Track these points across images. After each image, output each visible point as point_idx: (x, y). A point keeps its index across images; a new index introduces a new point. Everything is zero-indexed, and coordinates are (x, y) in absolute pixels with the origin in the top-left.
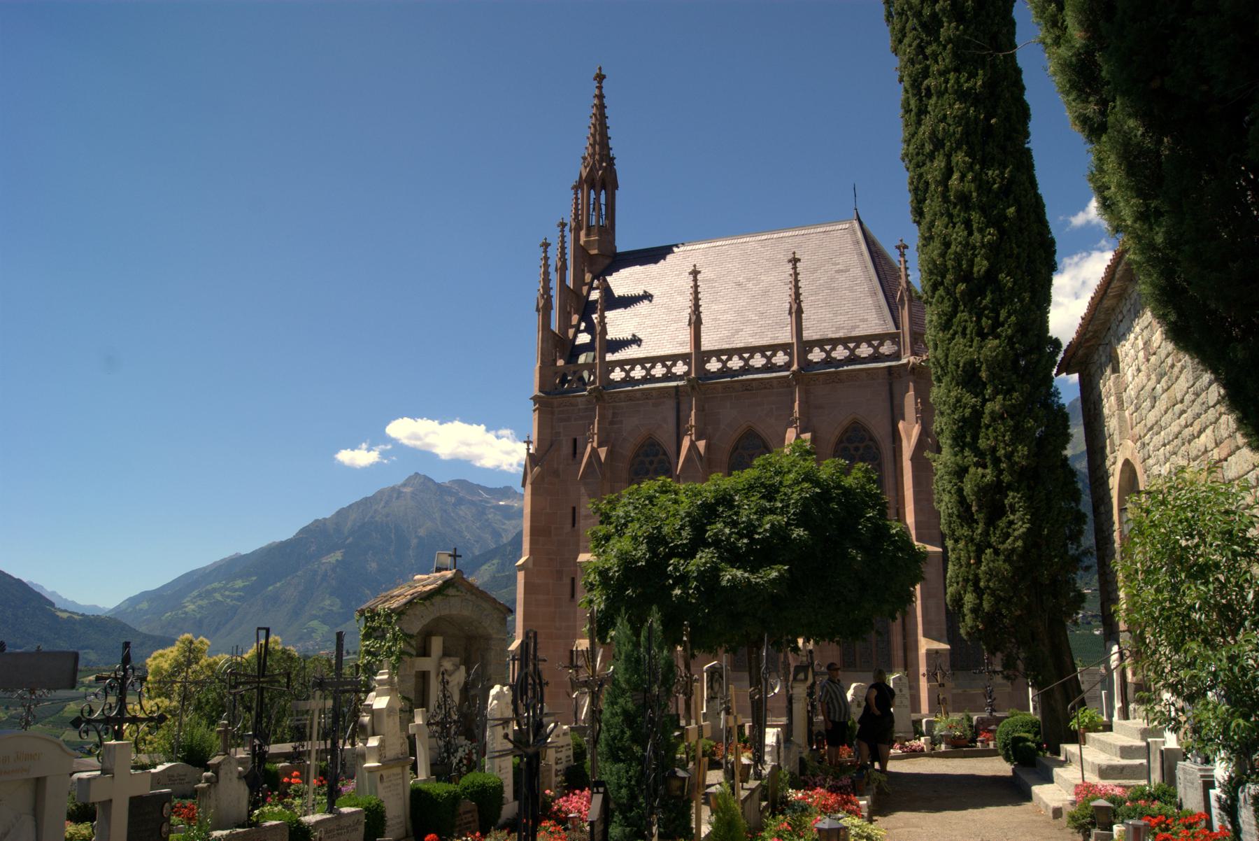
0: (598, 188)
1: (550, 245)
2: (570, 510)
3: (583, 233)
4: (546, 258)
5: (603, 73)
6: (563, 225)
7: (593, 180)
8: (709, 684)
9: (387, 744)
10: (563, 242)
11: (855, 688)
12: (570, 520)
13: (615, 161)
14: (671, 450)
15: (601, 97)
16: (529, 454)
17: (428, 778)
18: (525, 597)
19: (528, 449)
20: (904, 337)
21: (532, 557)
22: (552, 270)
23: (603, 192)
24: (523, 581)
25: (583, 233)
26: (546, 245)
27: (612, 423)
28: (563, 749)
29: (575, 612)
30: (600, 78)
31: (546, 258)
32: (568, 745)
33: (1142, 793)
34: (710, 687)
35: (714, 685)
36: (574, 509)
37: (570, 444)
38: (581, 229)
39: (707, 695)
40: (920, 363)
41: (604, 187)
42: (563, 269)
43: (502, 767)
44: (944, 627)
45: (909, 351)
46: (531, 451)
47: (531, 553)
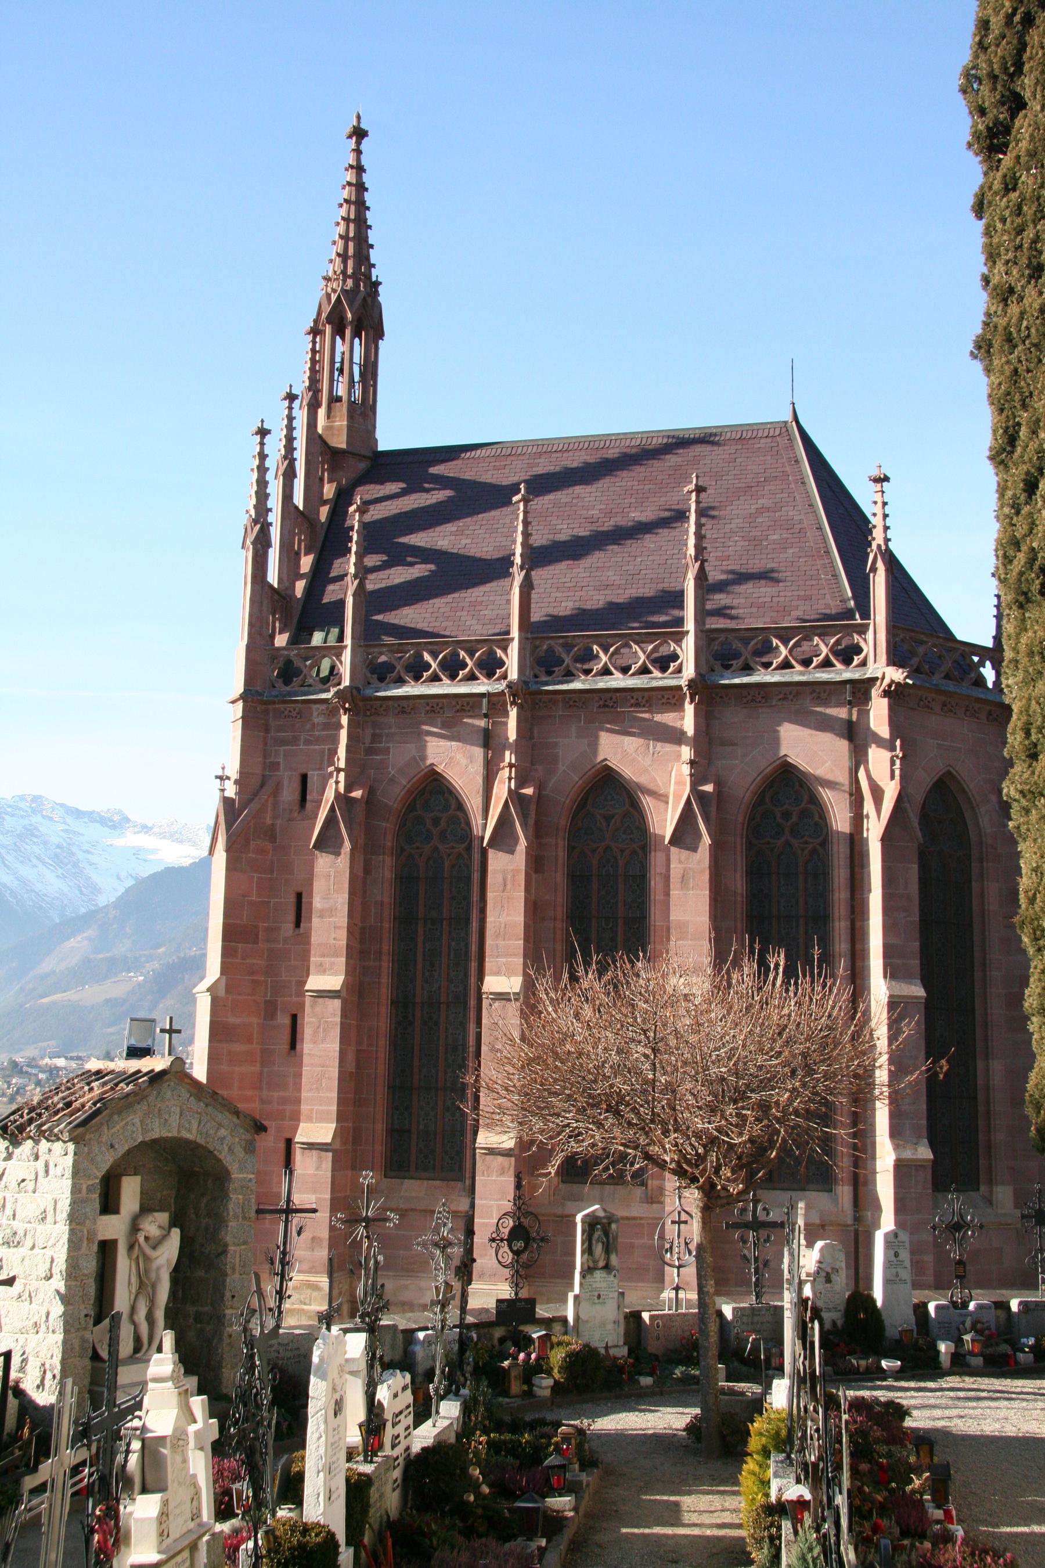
0: (348, 333)
1: (268, 432)
2: (292, 899)
4: (263, 456)
5: (363, 126)
6: (291, 397)
8: (586, 1245)
10: (290, 428)
12: (291, 917)
13: (380, 289)
14: (473, 802)
18: (210, 1047)
26: (263, 432)
27: (370, 751)
28: (402, 1417)
30: (359, 134)
31: (263, 456)
34: (588, 1250)
35: (594, 1247)
36: (299, 896)
39: (582, 1264)
46: (227, 794)
47: (225, 969)
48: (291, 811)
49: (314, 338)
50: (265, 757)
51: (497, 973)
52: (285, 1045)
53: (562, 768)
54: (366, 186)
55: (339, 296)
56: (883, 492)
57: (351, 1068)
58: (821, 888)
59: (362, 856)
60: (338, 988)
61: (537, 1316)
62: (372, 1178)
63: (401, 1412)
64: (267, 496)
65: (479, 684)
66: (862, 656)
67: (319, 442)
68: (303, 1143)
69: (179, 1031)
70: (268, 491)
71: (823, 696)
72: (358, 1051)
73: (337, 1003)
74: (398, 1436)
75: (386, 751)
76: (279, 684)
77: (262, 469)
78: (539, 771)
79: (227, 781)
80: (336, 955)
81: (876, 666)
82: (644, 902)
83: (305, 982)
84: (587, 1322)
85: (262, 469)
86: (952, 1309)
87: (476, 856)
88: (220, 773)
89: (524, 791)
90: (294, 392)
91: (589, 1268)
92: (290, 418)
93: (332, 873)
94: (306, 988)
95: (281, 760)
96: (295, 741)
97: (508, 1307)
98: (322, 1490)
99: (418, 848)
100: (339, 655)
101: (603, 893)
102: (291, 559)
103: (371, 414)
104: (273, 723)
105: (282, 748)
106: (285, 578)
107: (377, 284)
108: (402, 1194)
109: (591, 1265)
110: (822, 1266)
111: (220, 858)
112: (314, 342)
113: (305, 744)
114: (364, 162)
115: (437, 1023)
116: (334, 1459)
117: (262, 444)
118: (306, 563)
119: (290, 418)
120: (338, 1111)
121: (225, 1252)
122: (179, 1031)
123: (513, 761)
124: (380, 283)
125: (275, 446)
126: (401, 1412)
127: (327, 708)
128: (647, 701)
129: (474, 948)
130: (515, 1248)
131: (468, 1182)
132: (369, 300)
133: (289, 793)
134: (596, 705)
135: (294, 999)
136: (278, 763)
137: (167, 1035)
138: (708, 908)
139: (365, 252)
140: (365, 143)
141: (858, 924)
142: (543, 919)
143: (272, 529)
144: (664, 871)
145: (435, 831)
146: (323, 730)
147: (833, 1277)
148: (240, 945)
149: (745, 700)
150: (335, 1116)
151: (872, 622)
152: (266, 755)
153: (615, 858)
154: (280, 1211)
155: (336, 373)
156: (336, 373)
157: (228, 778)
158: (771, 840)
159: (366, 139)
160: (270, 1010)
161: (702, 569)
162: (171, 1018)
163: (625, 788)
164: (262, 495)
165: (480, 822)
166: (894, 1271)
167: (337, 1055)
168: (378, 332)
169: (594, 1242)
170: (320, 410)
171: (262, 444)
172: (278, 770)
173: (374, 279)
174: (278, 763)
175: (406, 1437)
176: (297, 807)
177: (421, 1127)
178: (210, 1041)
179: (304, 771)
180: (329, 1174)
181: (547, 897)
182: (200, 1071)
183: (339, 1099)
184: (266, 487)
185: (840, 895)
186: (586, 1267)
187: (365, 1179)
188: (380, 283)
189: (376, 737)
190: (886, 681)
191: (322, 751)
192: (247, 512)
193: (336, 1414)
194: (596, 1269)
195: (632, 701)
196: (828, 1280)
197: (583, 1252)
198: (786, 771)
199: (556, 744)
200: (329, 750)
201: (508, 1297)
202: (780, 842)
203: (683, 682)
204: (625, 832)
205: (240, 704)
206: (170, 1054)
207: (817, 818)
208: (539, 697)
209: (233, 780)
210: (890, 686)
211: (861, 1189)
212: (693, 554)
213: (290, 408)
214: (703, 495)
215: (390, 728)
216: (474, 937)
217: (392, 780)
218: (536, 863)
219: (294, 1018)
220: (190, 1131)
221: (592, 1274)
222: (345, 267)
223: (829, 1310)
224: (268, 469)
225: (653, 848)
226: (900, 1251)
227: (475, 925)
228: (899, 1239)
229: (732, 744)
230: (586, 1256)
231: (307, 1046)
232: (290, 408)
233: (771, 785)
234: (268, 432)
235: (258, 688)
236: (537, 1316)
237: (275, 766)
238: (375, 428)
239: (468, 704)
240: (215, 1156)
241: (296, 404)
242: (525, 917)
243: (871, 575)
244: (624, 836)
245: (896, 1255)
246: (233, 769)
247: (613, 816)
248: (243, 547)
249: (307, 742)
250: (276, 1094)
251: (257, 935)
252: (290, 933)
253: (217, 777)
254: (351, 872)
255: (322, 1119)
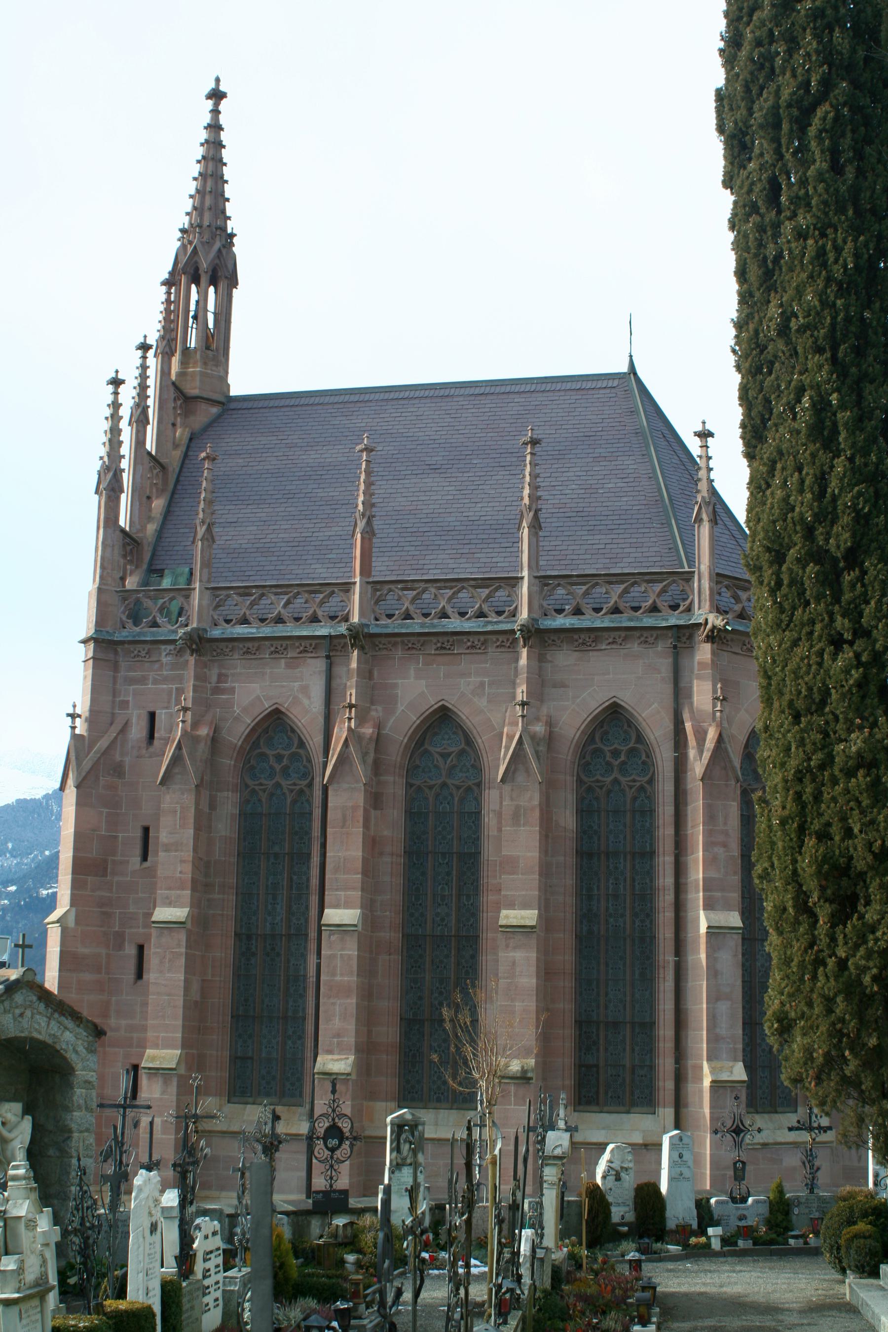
0: (204, 280)
1: (122, 382)
2: (139, 834)
3: (175, 361)
4: (116, 405)
5: (222, 88)
6: (144, 347)
7: (197, 269)
8: (394, 1145)
9: (26, 1265)
10: (143, 377)
11: (612, 1151)
12: (138, 850)
13: (235, 240)
14: (315, 741)
15: (215, 127)
16: (74, 737)
17: (57, 1306)
18: (60, 976)
19: (73, 728)
20: (699, 581)
21: (74, 909)
22: (124, 425)
23: (212, 289)
24: (58, 949)
25: (175, 361)
26: (116, 382)
27: (217, 690)
28: (212, 1256)
29: (145, 1004)
30: (217, 95)
31: (116, 405)
32: (218, 1249)
33: (808, 897)
34: (397, 1149)
35: (402, 1146)
36: (146, 830)
37: (144, 723)
38: (172, 353)
39: (391, 1161)
40: (724, 626)
41: (214, 281)
42: (140, 419)
43: (150, 1288)
44: (740, 1046)
45: (708, 603)
46: (77, 731)
47: (74, 902)
48: (140, 748)
49: (170, 289)
50: (114, 696)
51: (337, 906)
52: (131, 975)
53: (400, 708)
54: (224, 143)
55: (195, 247)
56: (708, 447)
57: (195, 995)
58: (648, 824)
59: (208, 793)
60: (184, 920)
61: (350, 1206)
62: (200, 1080)
63: (211, 1252)
64: (120, 443)
65: (322, 627)
66: (687, 602)
67: (172, 389)
68: (150, 1069)
69: (30, 947)
70: (121, 438)
71: (651, 640)
72: (203, 981)
73: (183, 936)
74: (209, 1270)
75: (232, 691)
76: (129, 624)
77: (115, 417)
78: (377, 712)
79: (78, 720)
80: (183, 888)
81: (700, 612)
82: (478, 838)
83: (152, 914)
84: (396, 1212)
85: (115, 417)
86: (731, 1204)
87: (317, 793)
88: (71, 711)
89: (363, 730)
90: (148, 342)
91: (398, 1164)
92: (144, 367)
93: (179, 809)
94: (154, 919)
95: (130, 699)
96: (143, 680)
97: (323, 1197)
98: (141, 1287)
99: (261, 784)
100: (187, 597)
101: (440, 829)
102: (142, 498)
103: (223, 360)
104: (123, 665)
105: (131, 687)
106: (136, 519)
107: (232, 236)
108: (245, 1118)
109: (399, 1161)
110: (613, 1165)
111: (71, 793)
112: (169, 293)
113: (153, 683)
114: (223, 120)
115: (278, 955)
116: (151, 1266)
117: (116, 393)
118: (158, 504)
119: (144, 367)
120: (183, 1037)
121: (69, 1138)
122: (30, 947)
123: (353, 702)
124: (235, 235)
125: (128, 395)
126: (211, 1252)
127: (175, 649)
128: (482, 644)
129: (315, 881)
130: (330, 1146)
131: (308, 1107)
132: (224, 251)
133: (137, 731)
134: (434, 647)
135: (141, 930)
136: (127, 702)
137: (20, 950)
138: (537, 844)
139: (221, 207)
140: (224, 105)
141: (682, 859)
142: (381, 854)
143: (125, 476)
144: (497, 808)
145: (278, 767)
146: (171, 670)
147: (623, 1175)
148: (89, 878)
149: (576, 643)
150: (179, 1043)
151: (696, 570)
152: (115, 694)
153: (451, 795)
154: (119, 1106)
155: (191, 320)
156: (191, 320)
157: (79, 716)
158: (600, 778)
159: (225, 100)
160: (119, 940)
161: (536, 517)
162: (24, 935)
163: (461, 727)
164: (114, 442)
165: (322, 759)
166: (678, 1170)
167: (182, 984)
168: (233, 282)
169: (402, 1141)
170: (174, 359)
171: (116, 393)
172: (127, 708)
173: (229, 231)
174: (127, 702)
175: (216, 1273)
176: (144, 745)
177: (264, 1055)
178: (60, 970)
179: (152, 710)
180: (174, 1098)
181: (385, 833)
182: (51, 980)
183: (184, 1026)
184: (120, 435)
185: (665, 831)
186: (394, 1163)
187: (194, 1081)
188: (235, 235)
189: (221, 678)
190: (709, 626)
191: (170, 692)
192: (101, 458)
193: (151, 1233)
194: (404, 1165)
195: (469, 644)
196: (618, 1178)
197: (392, 1151)
198: (615, 712)
199: (395, 686)
200: (177, 689)
201: (324, 1189)
202: (609, 779)
203: (516, 627)
204: (461, 771)
205: (91, 661)
206: (23, 966)
207: (644, 757)
208: (379, 639)
209: (83, 717)
210: (712, 630)
211: (683, 1111)
212: (528, 503)
213: (144, 358)
214: (538, 448)
215: (236, 668)
216: (315, 872)
217: (237, 719)
218: (375, 799)
219: (141, 948)
220: (40, 1033)
221: (400, 1170)
222: (201, 219)
223: (618, 1205)
224: (121, 417)
225: (487, 785)
226: (684, 1153)
227: (315, 860)
228: (684, 1142)
229: (564, 686)
230: (395, 1154)
231: (151, 975)
232: (144, 358)
233: (601, 724)
234: (122, 382)
235: (108, 629)
236: (350, 1206)
237: (124, 704)
238: (227, 373)
239: (311, 645)
240: (61, 1054)
241: (151, 353)
242: (363, 851)
243: (696, 525)
244: (461, 774)
245: (681, 1156)
246: (83, 708)
247: (449, 754)
248: (96, 492)
249: (155, 682)
250: (123, 1022)
251: (105, 869)
252: (137, 866)
253: (69, 715)
254: (197, 808)
255: (168, 1044)
